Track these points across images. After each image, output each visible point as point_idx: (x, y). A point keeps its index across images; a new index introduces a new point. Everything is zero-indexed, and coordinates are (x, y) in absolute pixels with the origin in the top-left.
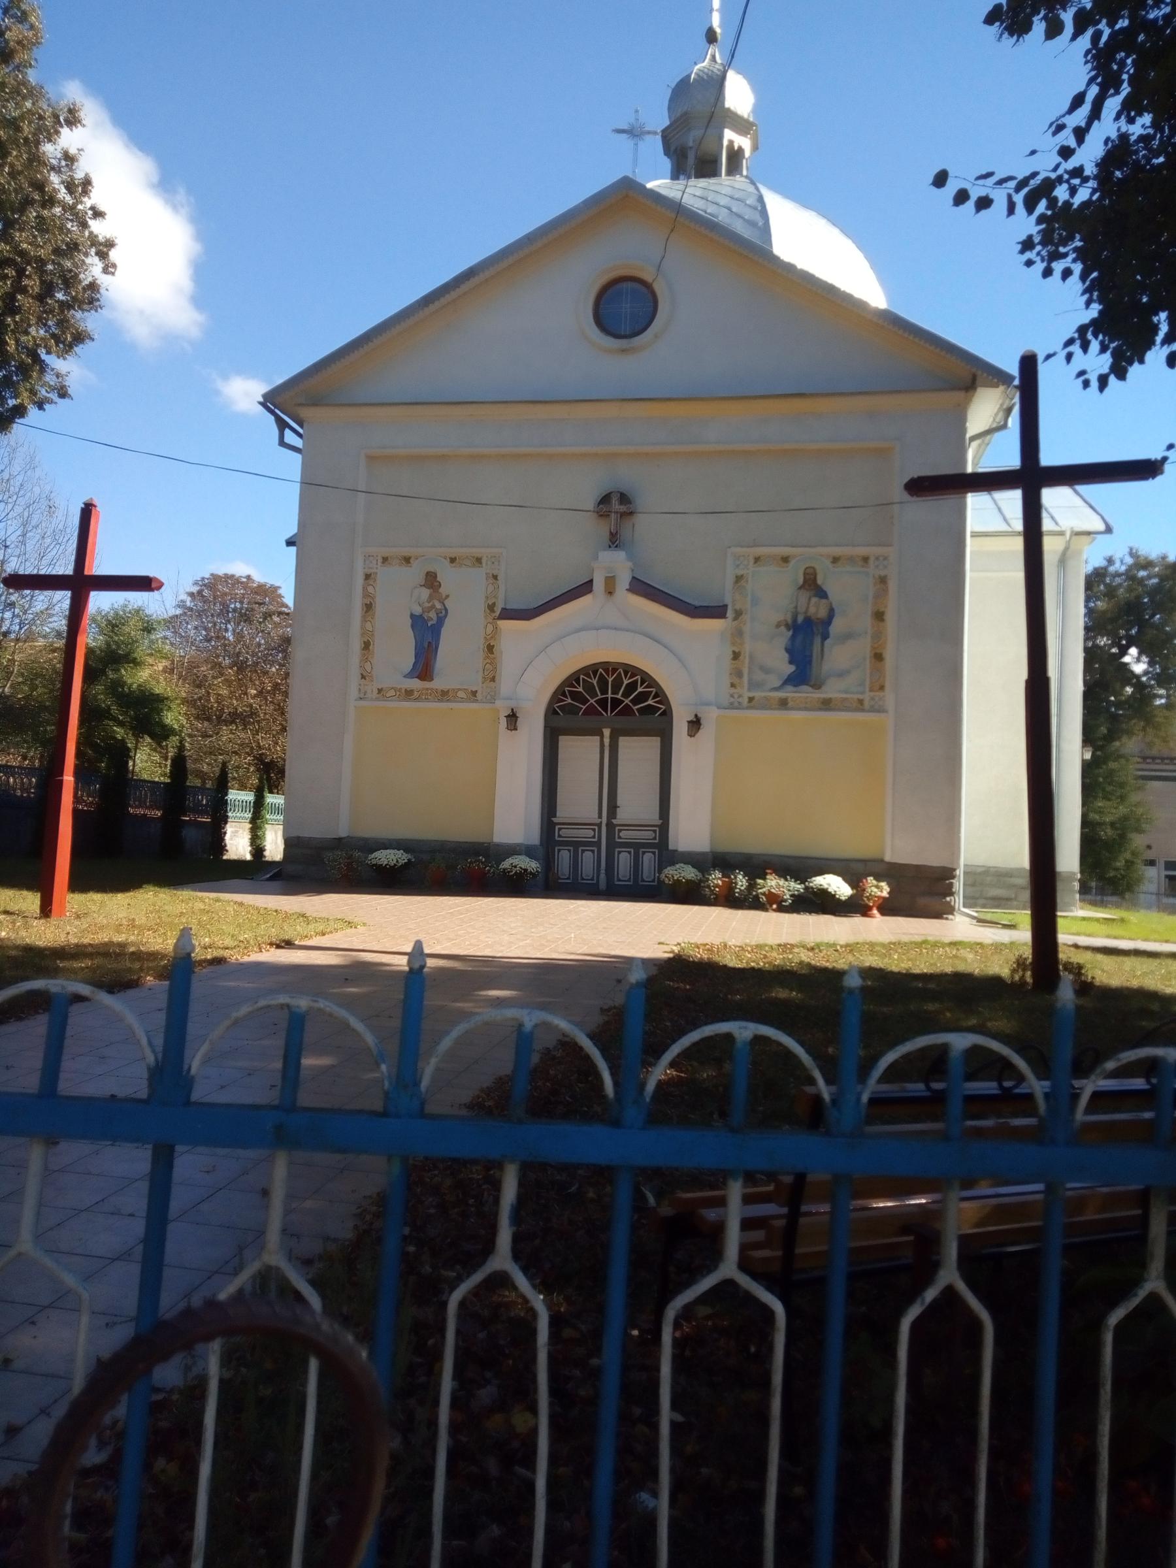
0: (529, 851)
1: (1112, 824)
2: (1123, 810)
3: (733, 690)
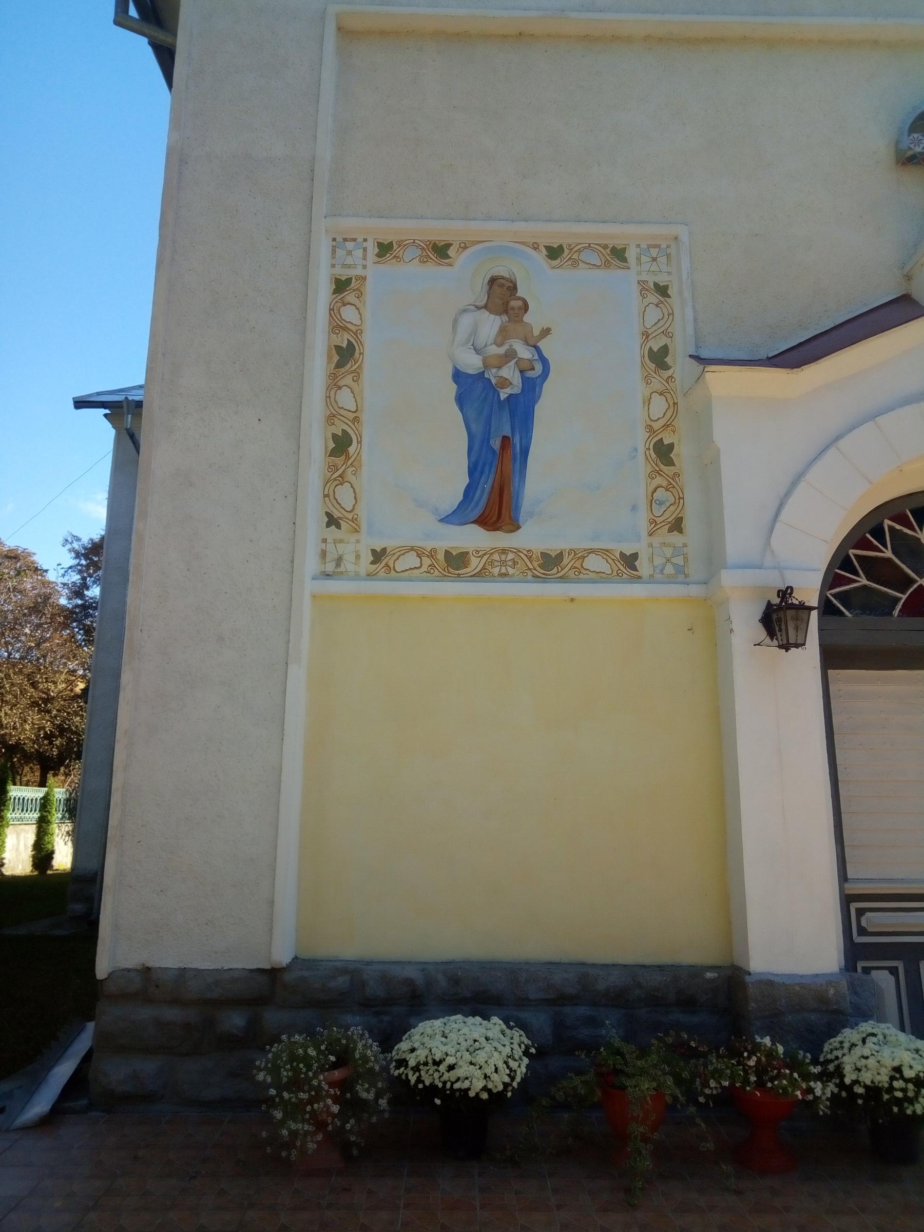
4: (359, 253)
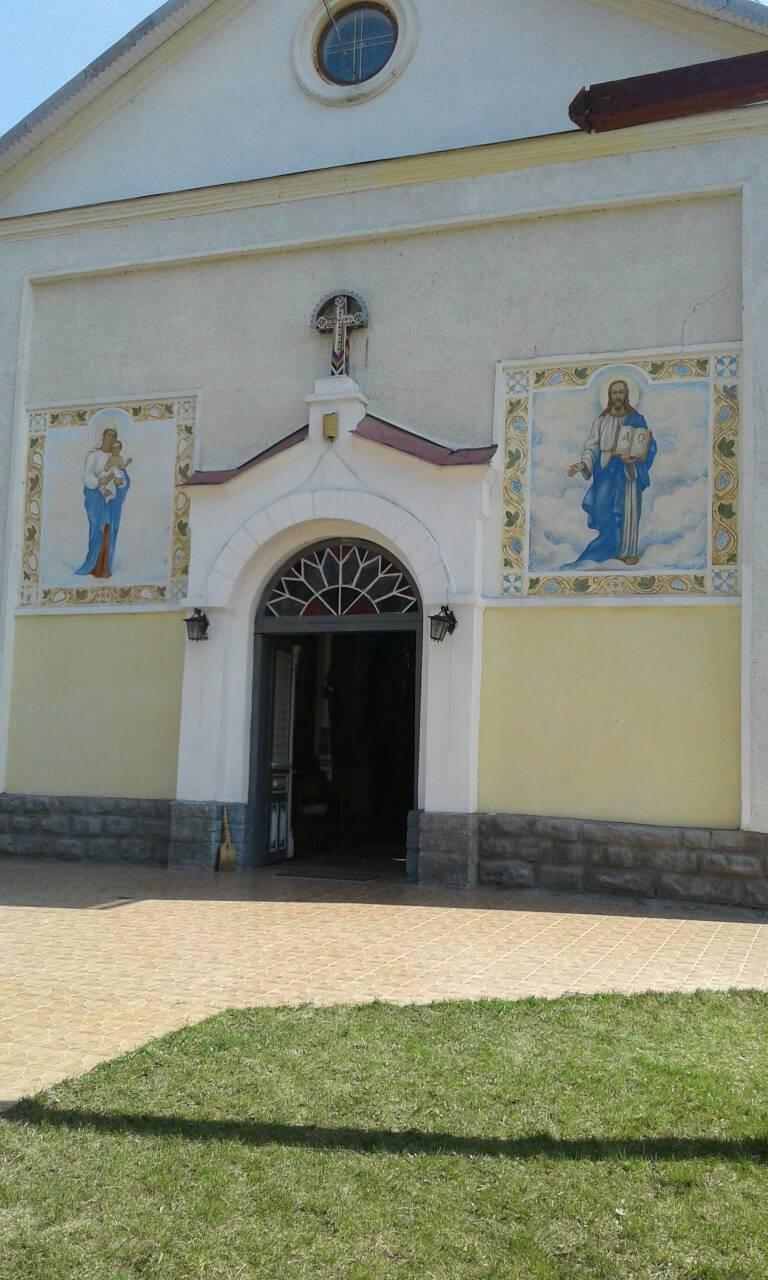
3: (507, 571)
4: (42, 422)
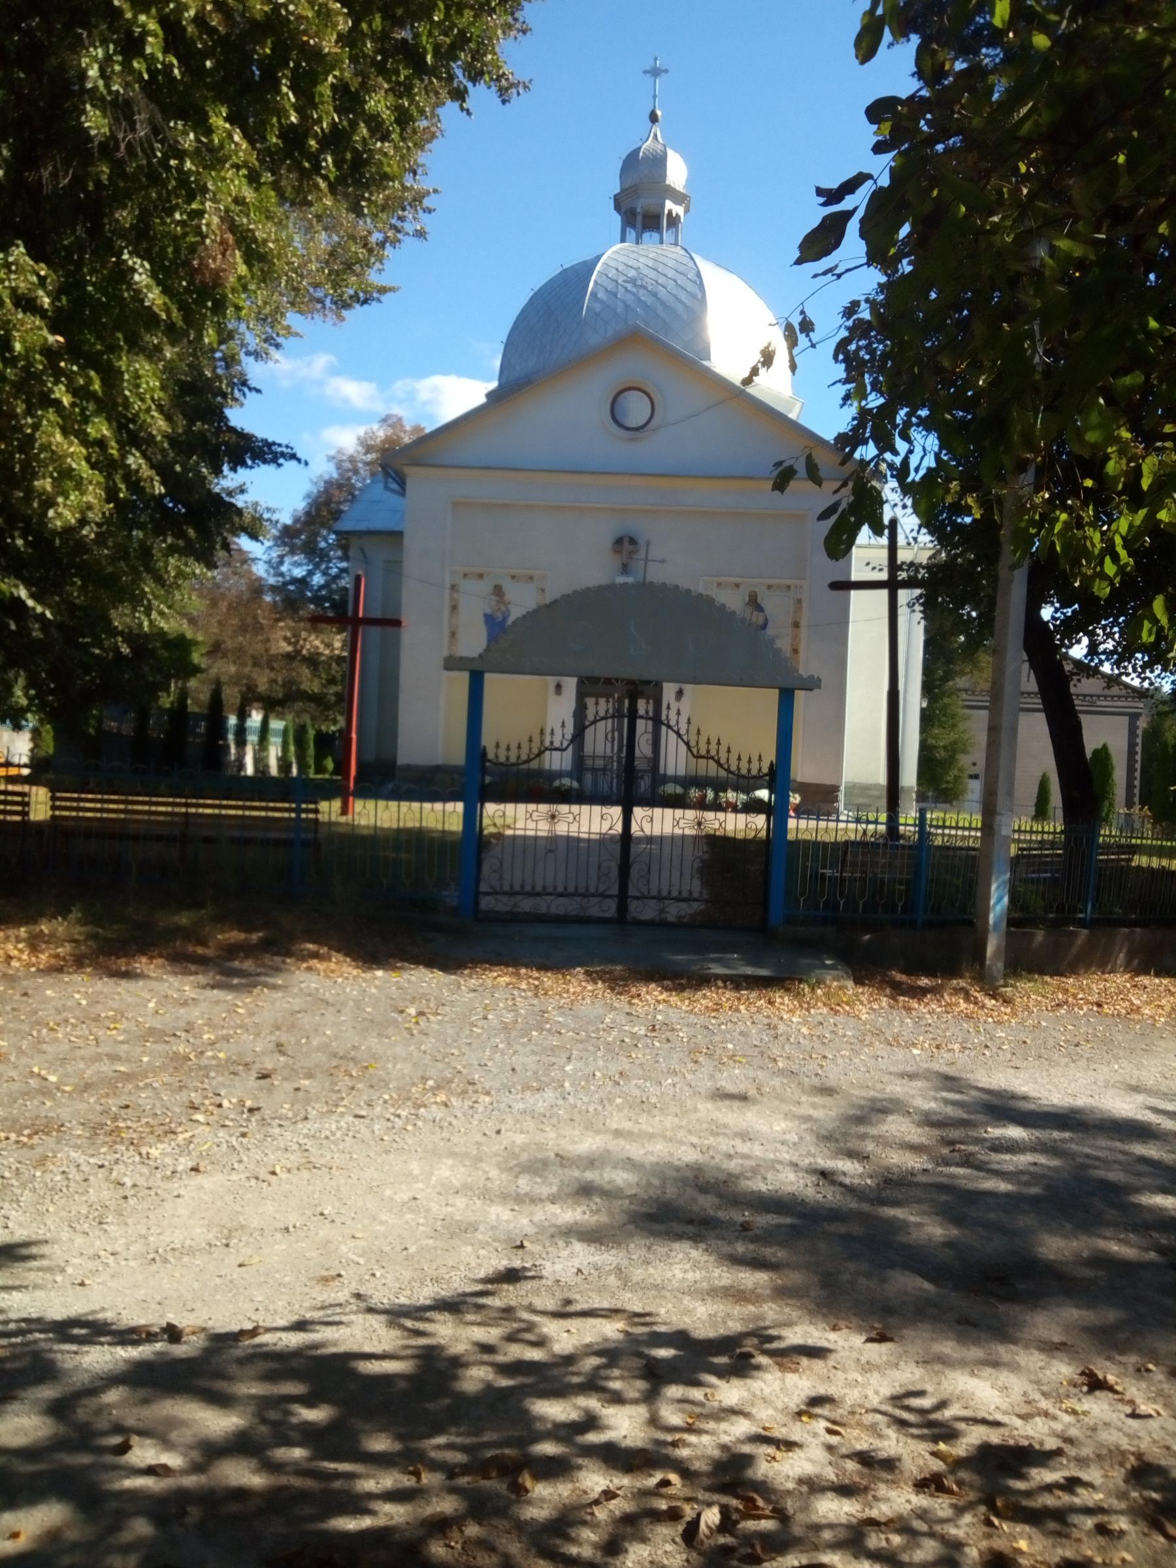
0: (569, 774)
1: (945, 747)
2: (953, 736)
